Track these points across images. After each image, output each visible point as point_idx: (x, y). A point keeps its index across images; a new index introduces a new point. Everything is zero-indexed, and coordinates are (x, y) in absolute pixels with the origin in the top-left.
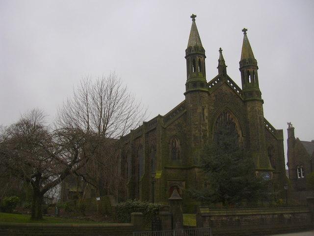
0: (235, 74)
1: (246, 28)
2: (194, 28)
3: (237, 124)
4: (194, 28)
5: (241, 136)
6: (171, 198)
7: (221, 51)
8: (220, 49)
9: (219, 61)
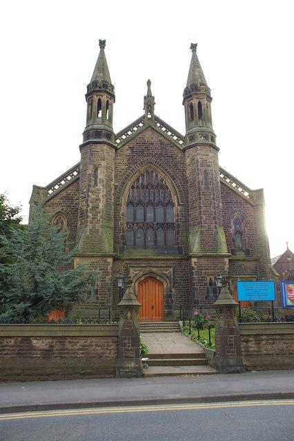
0: (173, 115)
1: (194, 43)
2: (195, 64)
3: (170, 187)
4: (195, 64)
5: (176, 204)
6: (219, 302)
7: (149, 83)
8: (149, 80)
9: (145, 98)
